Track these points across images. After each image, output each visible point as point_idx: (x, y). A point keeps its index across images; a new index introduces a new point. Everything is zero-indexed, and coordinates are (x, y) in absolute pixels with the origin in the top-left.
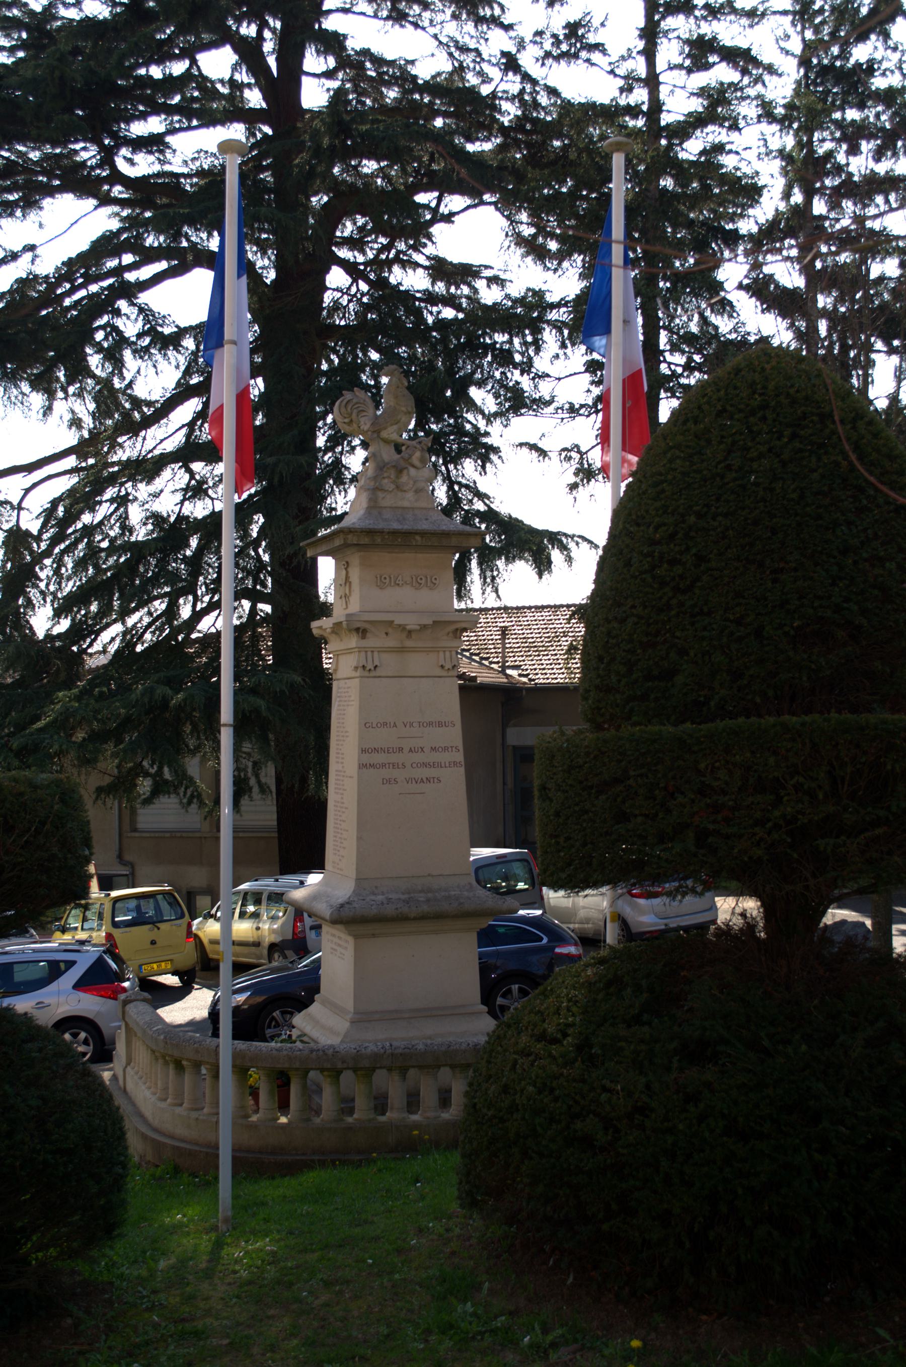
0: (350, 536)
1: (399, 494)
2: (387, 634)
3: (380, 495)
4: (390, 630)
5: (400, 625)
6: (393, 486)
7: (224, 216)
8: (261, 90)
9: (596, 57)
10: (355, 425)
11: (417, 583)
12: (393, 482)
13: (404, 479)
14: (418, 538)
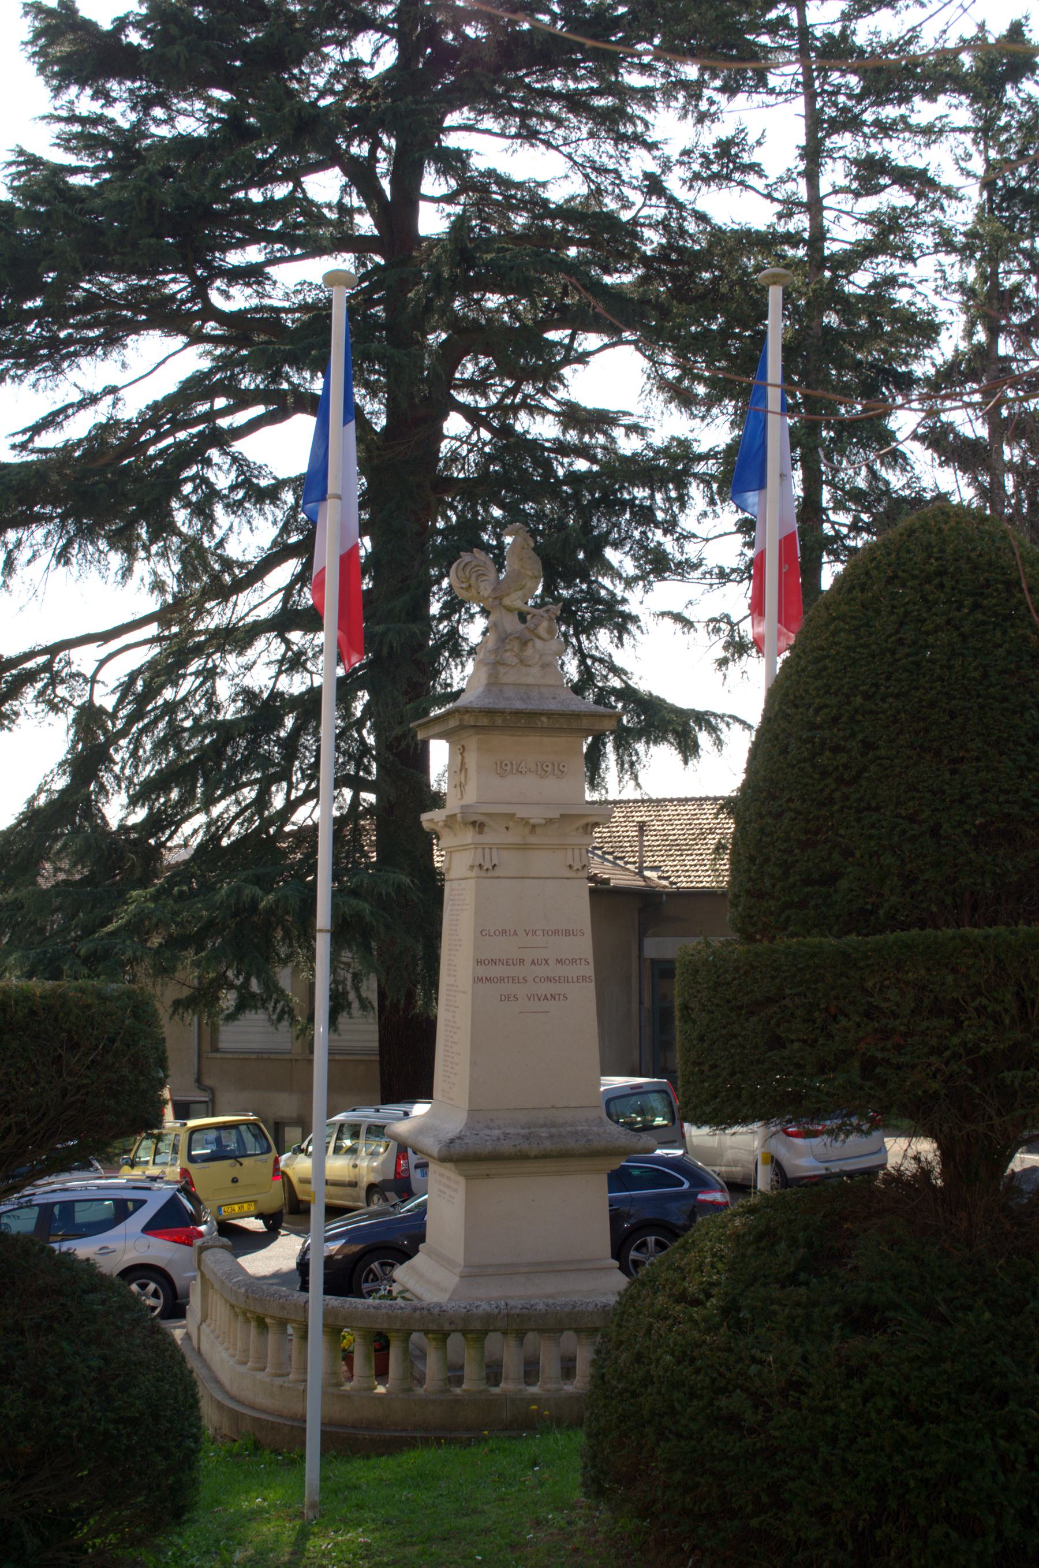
0: (467, 717)
3: (502, 670)
4: (511, 824)
5: (522, 819)
10: (474, 591)
13: (529, 652)
14: (544, 719)
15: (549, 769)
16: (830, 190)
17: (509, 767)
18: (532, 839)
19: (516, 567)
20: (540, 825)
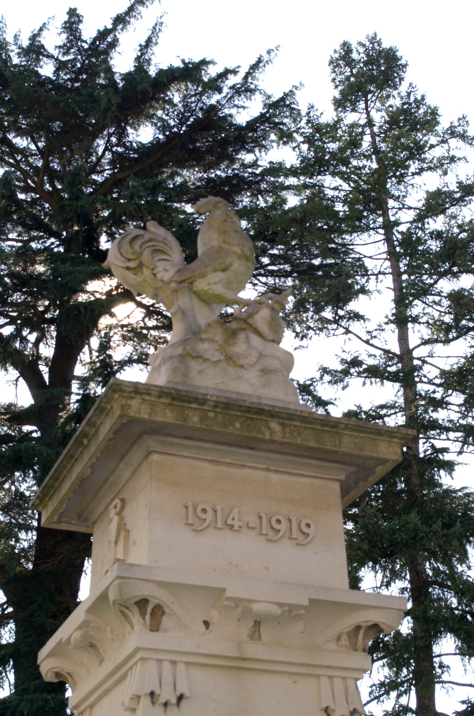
0: (135, 403)
1: (232, 370)
2: (207, 624)
3: (195, 365)
4: (214, 616)
5: (237, 601)
6: (217, 356)
7: (54, 631)
8: (73, 371)
9: (355, 326)
10: (147, 272)
11: (270, 530)
12: (221, 349)
13: (240, 347)
14: (274, 425)
15: (283, 527)
16: (419, 342)
17: (209, 516)
18: (254, 650)
19: (215, 243)
20: (270, 617)
